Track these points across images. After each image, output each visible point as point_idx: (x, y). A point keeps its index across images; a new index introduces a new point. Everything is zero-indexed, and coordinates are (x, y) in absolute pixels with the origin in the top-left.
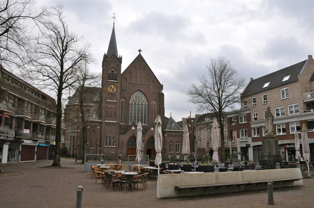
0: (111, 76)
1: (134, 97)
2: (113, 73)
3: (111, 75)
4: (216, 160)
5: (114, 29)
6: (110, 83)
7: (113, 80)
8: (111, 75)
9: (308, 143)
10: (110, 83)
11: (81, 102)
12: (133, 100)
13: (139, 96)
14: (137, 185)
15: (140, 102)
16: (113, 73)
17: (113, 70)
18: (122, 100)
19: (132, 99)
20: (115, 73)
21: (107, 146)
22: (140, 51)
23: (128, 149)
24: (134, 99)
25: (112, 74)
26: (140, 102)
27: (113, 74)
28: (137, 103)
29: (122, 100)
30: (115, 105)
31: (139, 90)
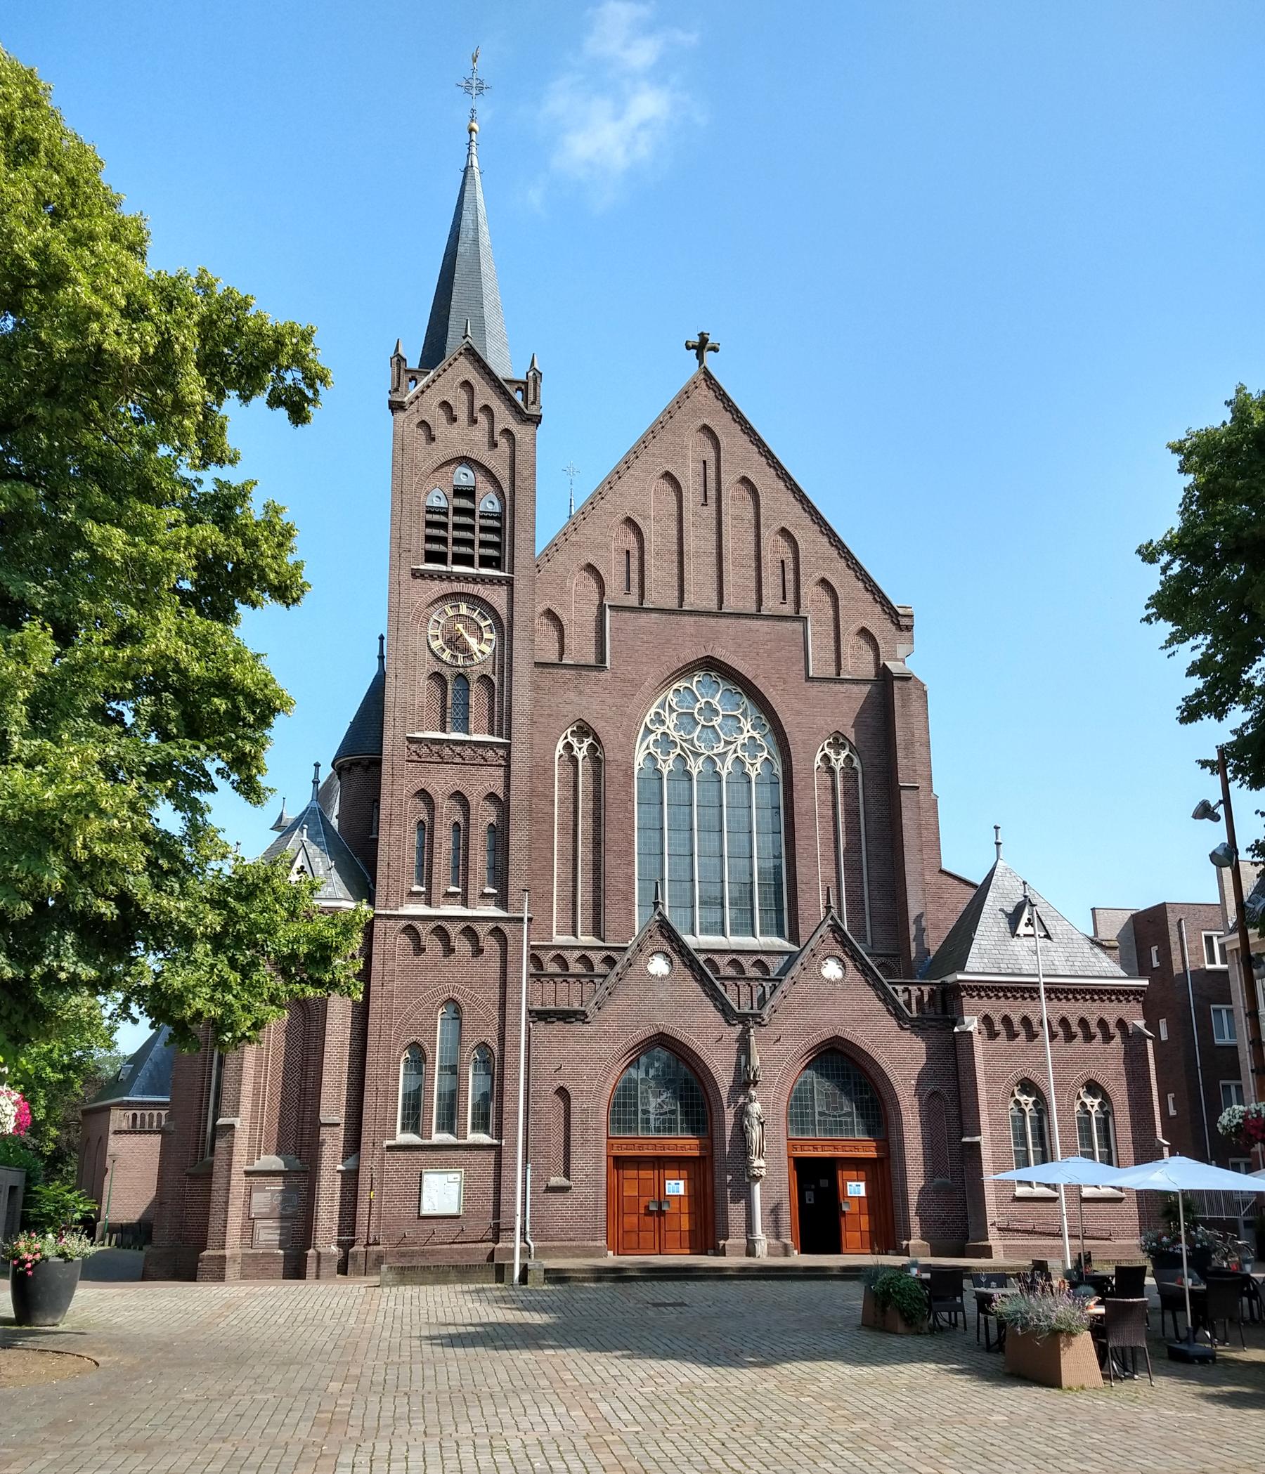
0: (451, 534)
1: (671, 720)
2: (464, 503)
3: (452, 519)
4: (318, 894)
5: (993, 869)
6: (447, 587)
7: (467, 560)
8: (452, 519)
9: (800, 1259)
10: (447, 587)
11: (73, 666)
12: (666, 742)
13: (711, 710)
14: (1175, 1321)
15: (723, 755)
16: (464, 503)
17: (464, 476)
18: (569, 747)
19: (652, 737)
20: (487, 502)
21: (484, 1139)
22: (701, 346)
23: (619, 1163)
24: (675, 735)
25: (458, 511)
26: (723, 755)
27: (470, 513)
28: (696, 766)
29: (569, 747)
30: (484, 771)
31: (710, 665)
